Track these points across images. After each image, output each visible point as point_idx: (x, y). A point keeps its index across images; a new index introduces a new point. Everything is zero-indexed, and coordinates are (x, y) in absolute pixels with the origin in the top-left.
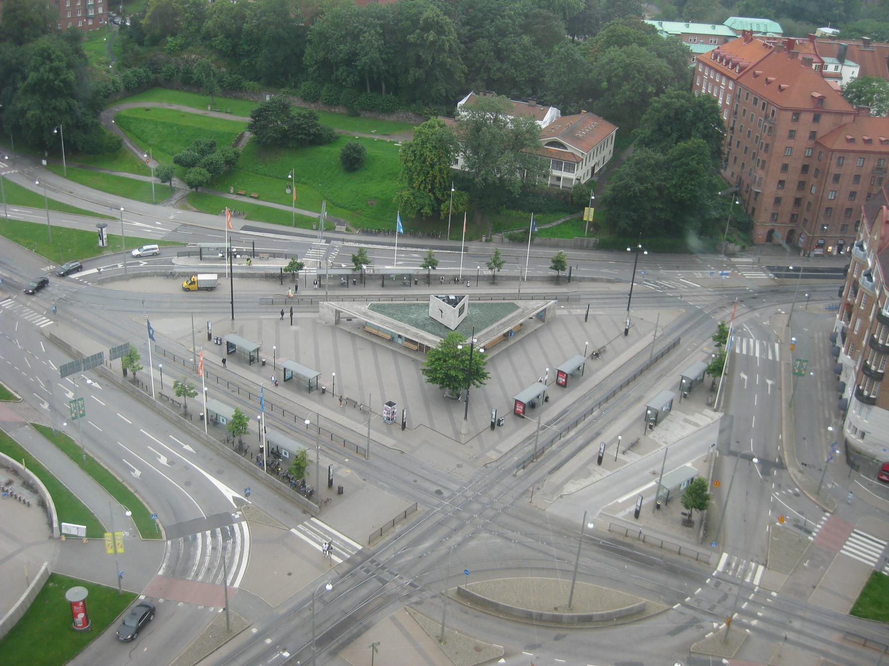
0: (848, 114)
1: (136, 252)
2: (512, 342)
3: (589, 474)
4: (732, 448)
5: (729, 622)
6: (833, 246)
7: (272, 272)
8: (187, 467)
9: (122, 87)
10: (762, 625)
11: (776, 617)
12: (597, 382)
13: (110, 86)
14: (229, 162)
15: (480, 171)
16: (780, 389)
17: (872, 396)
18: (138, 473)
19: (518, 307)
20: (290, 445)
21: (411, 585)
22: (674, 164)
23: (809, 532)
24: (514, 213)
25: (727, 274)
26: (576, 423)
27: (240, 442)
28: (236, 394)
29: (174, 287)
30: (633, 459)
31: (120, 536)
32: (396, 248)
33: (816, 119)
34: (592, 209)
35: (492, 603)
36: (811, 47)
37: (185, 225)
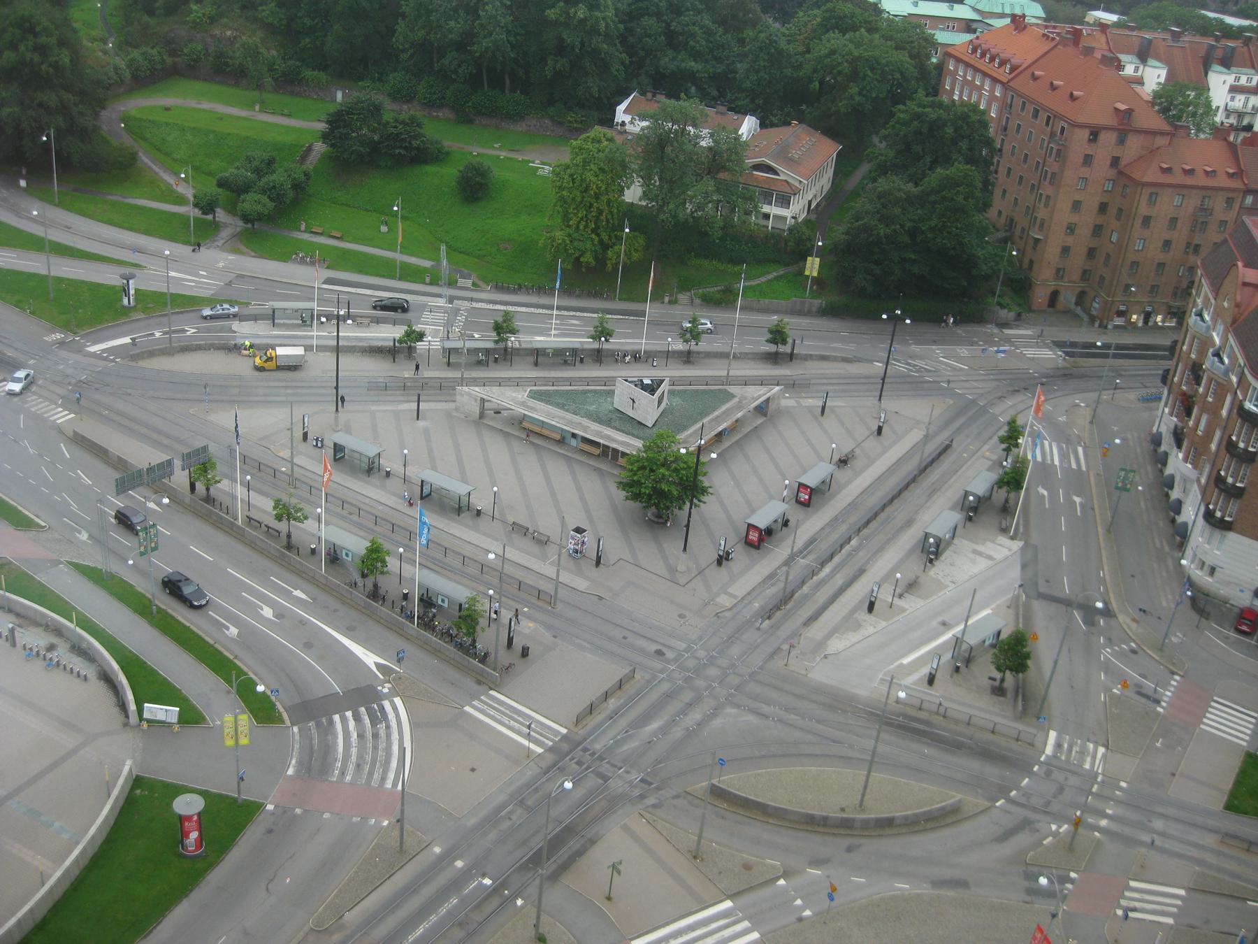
0: (1162, 133)
1: (207, 312)
2: (727, 443)
3: (858, 626)
4: (1042, 589)
5: (1077, 823)
6: (1139, 315)
7: (380, 344)
8: (303, 622)
9: (127, 74)
10: (1115, 827)
11: (1131, 815)
12: (849, 499)
13: (112, 74)
14: (297, 187)
15: (665, 203)
16: (1093, 509)
17: (1227, 519)
18: (233, 631)
19: (733, 396)
20: (452, 590)
21: (642, 780)
22: (932, 198)
23: (1158, 702)
24: (706, 263)
25: (1004, 352)
26: (832, 557)
27: (376, 586)
28: (355, 518)
29: (241, 366)
30: (912, 605)
31: (233, 723)
32: (555, 312)
33: (1121, 141)
34: (818, 260)
35: (759, 803)
36: (1103, 39)
37: (242, 276)
